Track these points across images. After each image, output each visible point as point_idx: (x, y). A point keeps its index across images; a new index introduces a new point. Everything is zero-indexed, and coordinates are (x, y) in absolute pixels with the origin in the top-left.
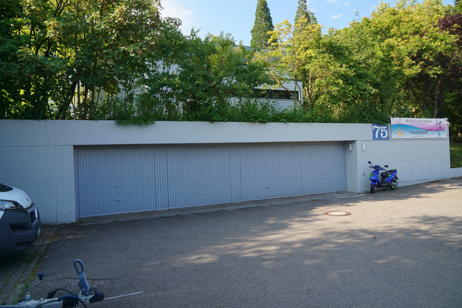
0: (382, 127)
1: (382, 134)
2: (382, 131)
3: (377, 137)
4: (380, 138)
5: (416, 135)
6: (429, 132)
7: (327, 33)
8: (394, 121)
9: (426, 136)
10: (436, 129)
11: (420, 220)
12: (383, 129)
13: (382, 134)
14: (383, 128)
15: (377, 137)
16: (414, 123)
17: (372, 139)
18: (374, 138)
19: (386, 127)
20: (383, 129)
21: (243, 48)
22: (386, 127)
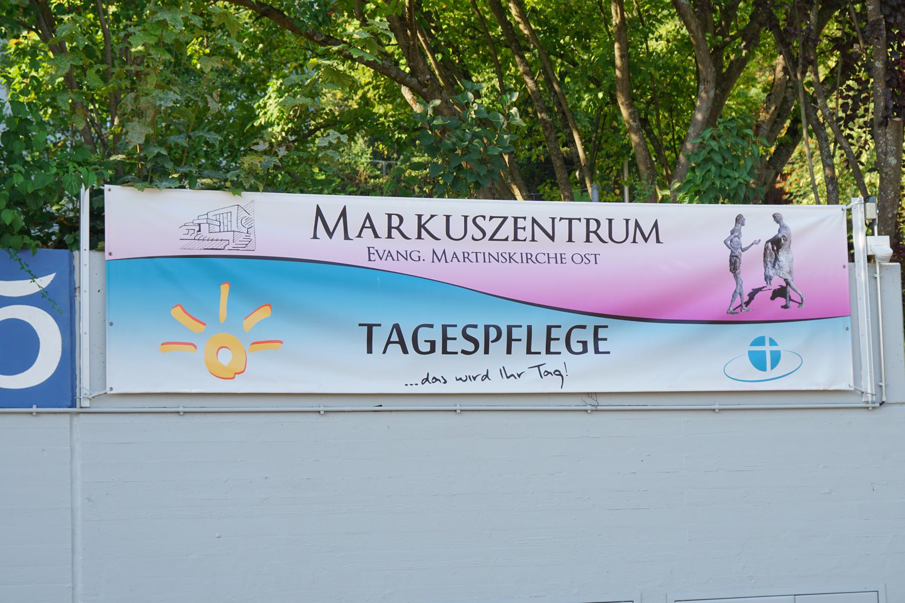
5: (437, 363)
6: (621, 339)
8: (145, 219)
10: (722, 298)
16: (426, 246)
19: (45, 281)
22: (45, 281)
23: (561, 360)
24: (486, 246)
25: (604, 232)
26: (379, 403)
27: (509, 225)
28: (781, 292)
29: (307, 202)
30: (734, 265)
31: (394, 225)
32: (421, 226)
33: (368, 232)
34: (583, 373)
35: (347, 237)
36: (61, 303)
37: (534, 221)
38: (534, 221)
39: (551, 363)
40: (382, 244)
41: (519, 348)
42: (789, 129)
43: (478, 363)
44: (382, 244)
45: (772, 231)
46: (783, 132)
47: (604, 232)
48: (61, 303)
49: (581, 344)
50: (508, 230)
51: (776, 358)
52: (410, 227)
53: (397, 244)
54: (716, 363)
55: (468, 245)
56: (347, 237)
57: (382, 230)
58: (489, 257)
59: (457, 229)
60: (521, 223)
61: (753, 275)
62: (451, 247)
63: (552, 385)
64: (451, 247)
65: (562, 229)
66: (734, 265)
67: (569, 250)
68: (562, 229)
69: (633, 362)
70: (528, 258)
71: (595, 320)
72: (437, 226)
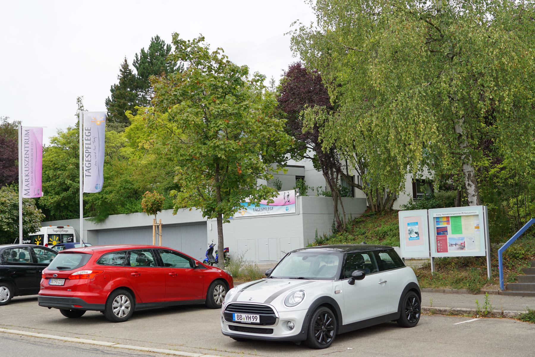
10: (283, 203)
24: (30, 163)
27: (26, 159)
31: (27, 181)
40: (30, 183)
42: (32, 233)
46: (339, 182)
47: (27, 141)
49: (164, 261)
50: (27, 159)
52: (27, 178)
55: (30, 167)
57: (28, 183)
58: (32, 163)
59: (27, 169)
61: (286, 200)
62: (30, 170)
65: (26, 149)
68: (26, 149)
70: (32, 155)
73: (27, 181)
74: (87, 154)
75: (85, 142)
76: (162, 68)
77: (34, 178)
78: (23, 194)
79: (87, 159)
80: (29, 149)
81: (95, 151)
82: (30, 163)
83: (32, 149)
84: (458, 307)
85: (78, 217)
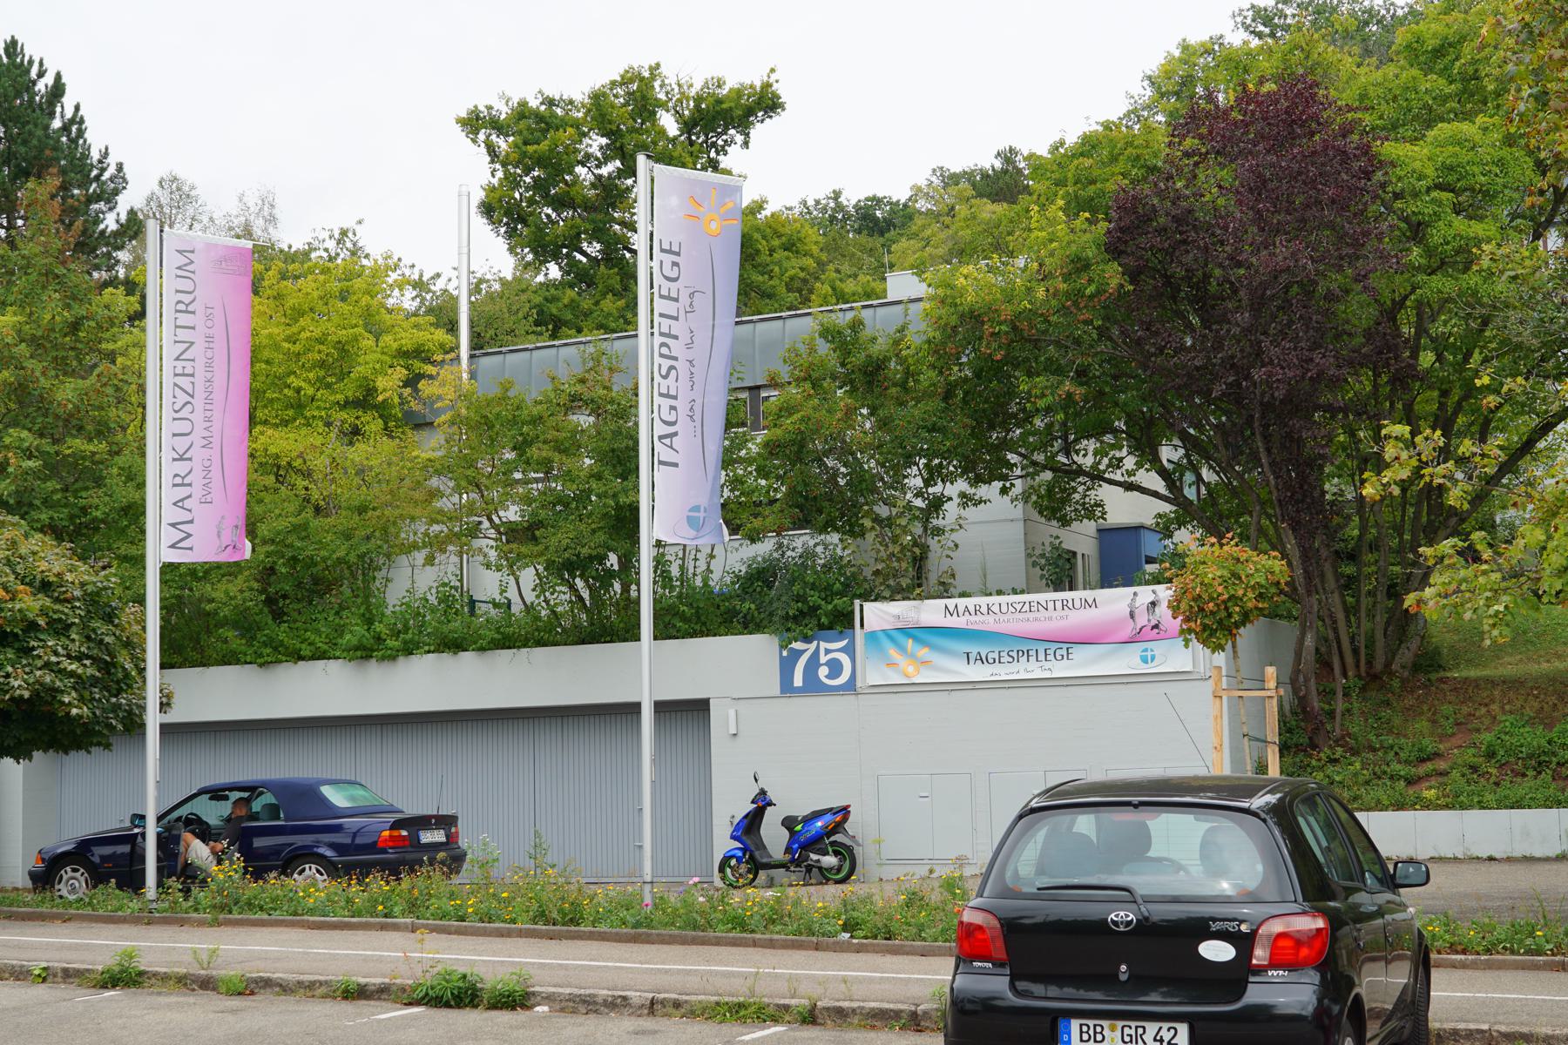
0: (823, 645)
1: (823, 672)
2: (823, 659)
3: (798, 681)
4: (813, 686)
5: (997, 668)
6: (1079, 653)
7: (787, 368)
8: (877, 614)
9: (1060, 669)
10: (1127, 632)
11: (675, 571)
12: (827, 651)
13: (823, 672)
14: (830, 648)
15: (798, 681)
16: (991, 618)
17: (777, 692)
18: (787, 687)
19: (844, 643)
20: (827, 651)
21: (502, 281)
22: (844, 643)
23: (1053, 664)
24: (198, 401)
25: (187, 298)
26: (973, 685)
27: (181, 381)
28: (1156, 627)
29: (941, 602)
30: (1132, 615)
31: (181, 482)
32: (181, 459)
33: (187, 504)
34: (1060, 669)
35: (191, 522)
36: (850, 651)
37: (177, 359)
38: (177, 359)
39: (1047, 665)
40: (197, 490)
41: (1033, 659)
43: (1015, 666)
44: (973, 618)
45: (1151, 598)
47: (187, 298)
48: (850, 651)
50: (1027, 607)
51: (1153, 659)
52: (182, 468)
53: (979, 618)
54: (1126, 661)
55: (198, 417)
56: (191, 522)
57: (184, 492)
58: (208, 401)
59: (183, 427)
60: (179, 371)
61: (1142, 619)
62: (199, 432)
63: (1047, 675)
64: (1003, 617)
65: (1051, 605)
66: (1132, 615)
67: (1055, 614)
68: (1051, 605)
69: (1084, 662)
70: (209, 366)
71: (1068, 642)
72: (995, 609)
73: (181, 482)
74: (666, 363)
75: (660, 306)
76: (47, 152)
77: (216, 473)
78: (165, 542)
79: (664, 383)
80: (197, 337)
81: (690, 355)
82: (198, 401)
83: (209, 339)
84: (1447, 1020)
85: (637, 638)
